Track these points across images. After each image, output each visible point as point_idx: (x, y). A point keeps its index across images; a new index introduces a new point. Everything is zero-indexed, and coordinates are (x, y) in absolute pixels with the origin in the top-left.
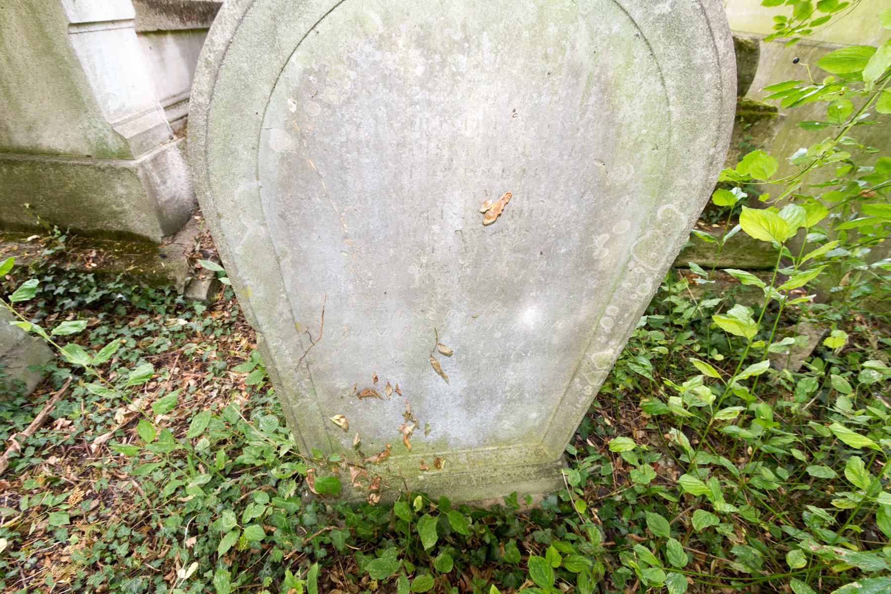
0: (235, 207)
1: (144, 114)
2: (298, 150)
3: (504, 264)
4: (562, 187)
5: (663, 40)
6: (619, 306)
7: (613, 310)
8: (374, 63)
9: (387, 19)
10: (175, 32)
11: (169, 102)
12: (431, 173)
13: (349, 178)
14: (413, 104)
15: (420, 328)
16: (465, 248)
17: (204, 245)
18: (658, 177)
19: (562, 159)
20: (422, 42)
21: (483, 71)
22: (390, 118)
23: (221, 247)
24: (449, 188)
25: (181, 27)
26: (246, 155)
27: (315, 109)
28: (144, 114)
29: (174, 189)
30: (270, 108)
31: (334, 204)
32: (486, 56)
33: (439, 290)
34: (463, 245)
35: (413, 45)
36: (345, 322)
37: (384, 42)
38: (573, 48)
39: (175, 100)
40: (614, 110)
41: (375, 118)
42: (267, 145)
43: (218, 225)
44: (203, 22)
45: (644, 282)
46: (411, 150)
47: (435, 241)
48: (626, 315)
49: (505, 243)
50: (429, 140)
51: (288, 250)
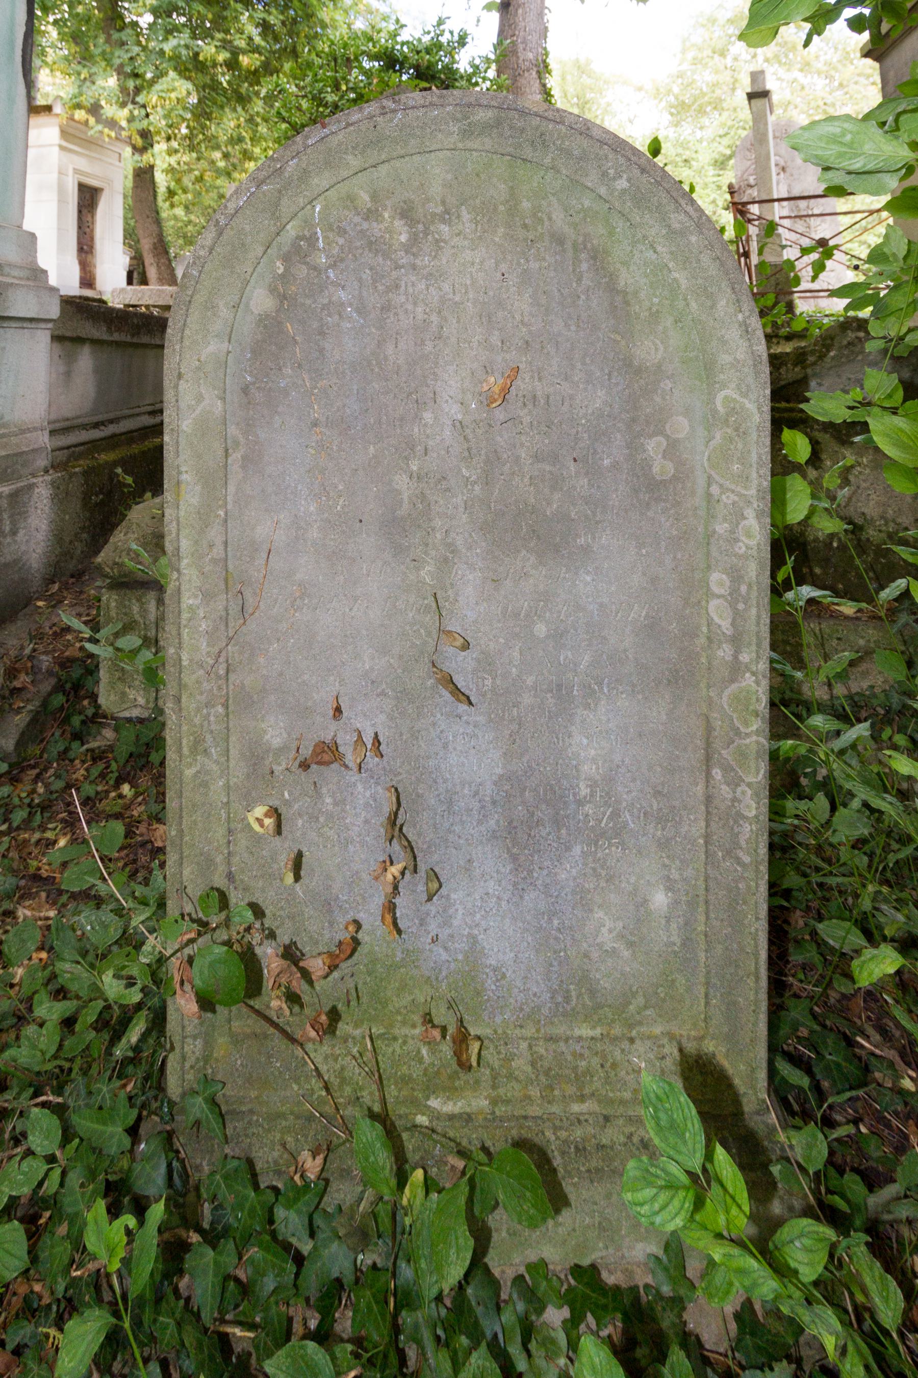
0: (199, 369)
1: (23, 432)
2: (278, 311)
3: (526, 480)
4: (579, 365)
5: (635, 210)
6: (725, 571)
7: (721, 584)
8: (361, 231)
9: (374, 197)
10: (95, 342)
11: (58, 426)
12: (419, 342)
13: (327, 346)
14: (398, 267)
15: (411, 600)
16: (469, 450)
17: (41, 648)
18: (697, 357)
19: (569, 330)
20: (406, 213)
21: (465, 238)
22: (375, 281)
23: (170, 416)
24: (441, 362)
25: (106, 337)
26: (224, 312)
27: (302, 271)
28: (23, 432)
29: (23, 548)
30: (259, 269)
31: (306, 376)
32: (467, 225)
33: (438, 523)
34: (466, 446)
35: (398, 217)
36: (298, 577)
37: (371, 215)
38: (550, 219)
39: (67, 424)
40: (612, 277)
41: (360, 280)
42: (247, 305)
43: (176, 387)
44: (133, 336)
45: (744, 518)
46: (396, 314)
47: (428, 437)
48: (743, 589)
49: (522, 445)
50: (415, 304)
51: (242, 440)
